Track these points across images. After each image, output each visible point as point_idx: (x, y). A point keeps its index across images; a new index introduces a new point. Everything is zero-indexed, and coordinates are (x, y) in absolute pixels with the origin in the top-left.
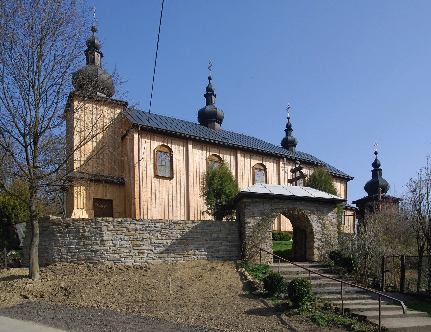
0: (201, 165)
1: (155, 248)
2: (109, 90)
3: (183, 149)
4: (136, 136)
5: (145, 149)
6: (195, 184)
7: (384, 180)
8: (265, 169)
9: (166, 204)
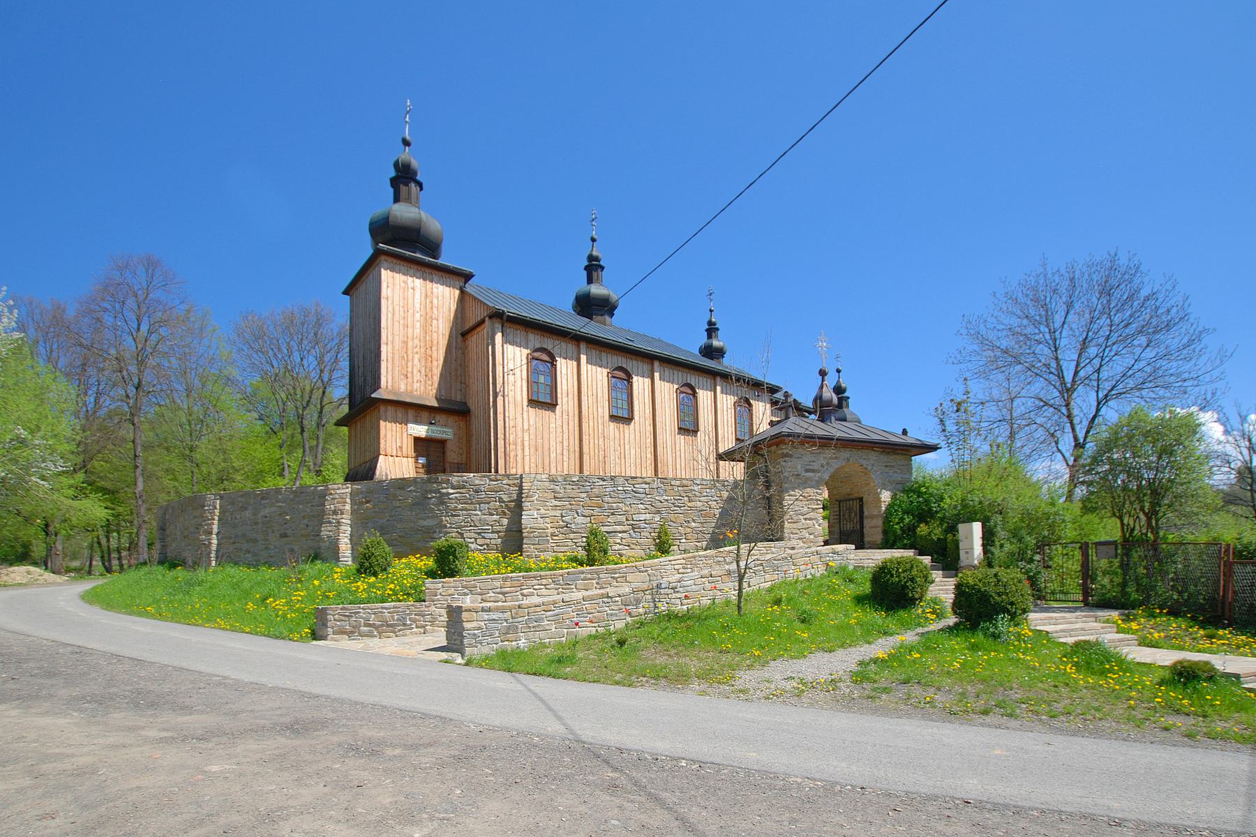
3: (710, 394)
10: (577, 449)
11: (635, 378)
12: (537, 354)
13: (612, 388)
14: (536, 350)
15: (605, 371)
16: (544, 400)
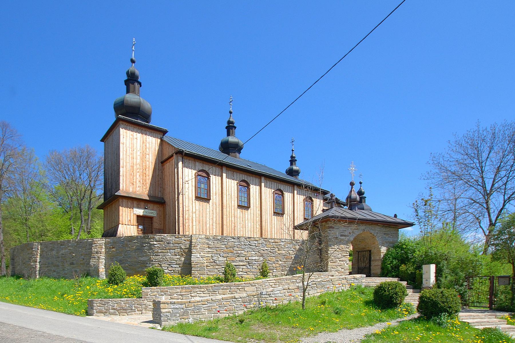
0: (233, 189)
1: (249, 264)
2: (146, 117)
3: (291, 195)
4: (180, 164)
5: (187, 176)
6: (228, 206)
7: (367, 206)
8: (312, 201)
9: (204, 221)
10: (220, 222)
11: (251, 186)
12: (199, 173)
13: (239, 191)
14: (199, 171)
15: (236, 182)
16: (203, 197)
